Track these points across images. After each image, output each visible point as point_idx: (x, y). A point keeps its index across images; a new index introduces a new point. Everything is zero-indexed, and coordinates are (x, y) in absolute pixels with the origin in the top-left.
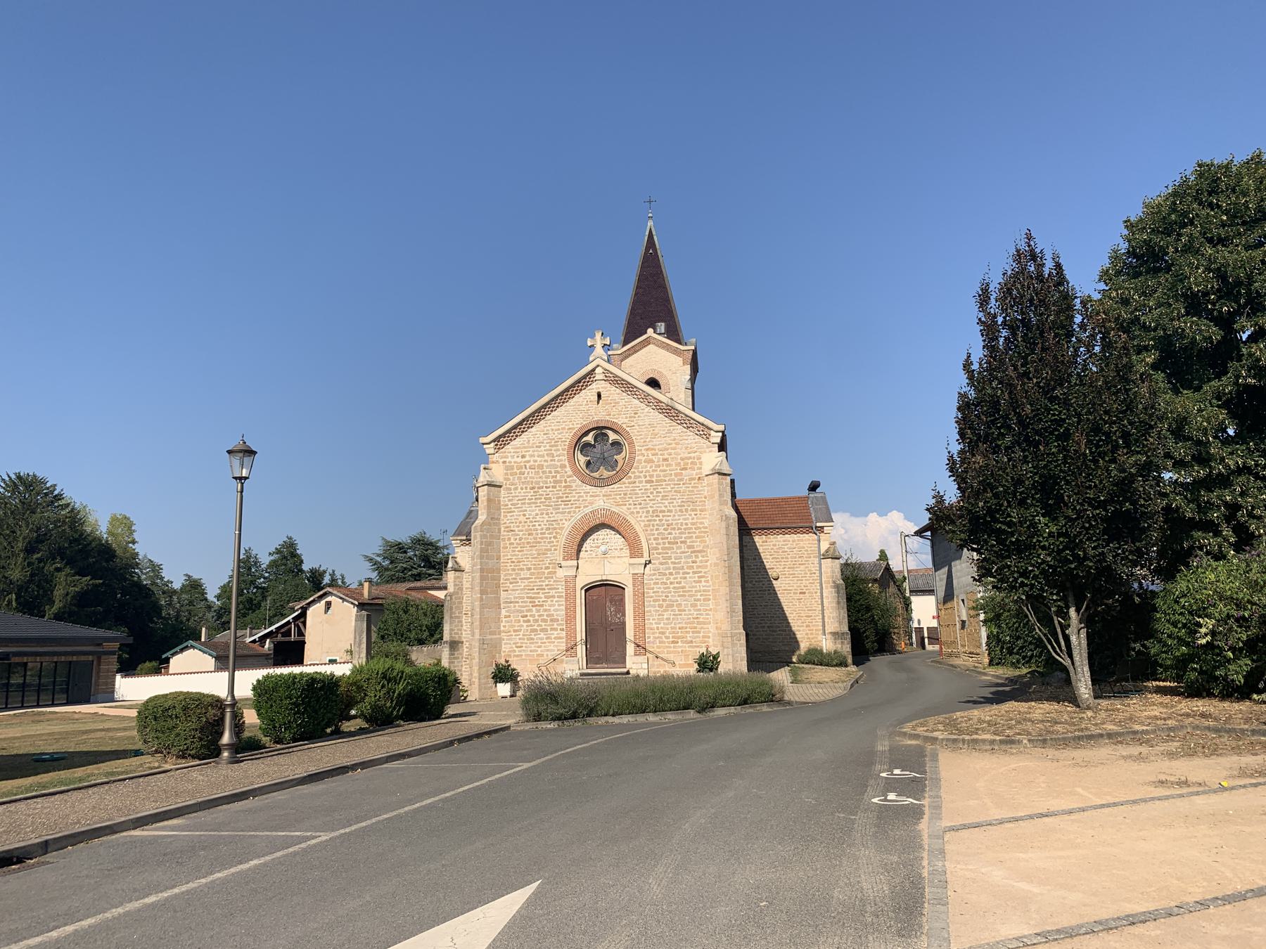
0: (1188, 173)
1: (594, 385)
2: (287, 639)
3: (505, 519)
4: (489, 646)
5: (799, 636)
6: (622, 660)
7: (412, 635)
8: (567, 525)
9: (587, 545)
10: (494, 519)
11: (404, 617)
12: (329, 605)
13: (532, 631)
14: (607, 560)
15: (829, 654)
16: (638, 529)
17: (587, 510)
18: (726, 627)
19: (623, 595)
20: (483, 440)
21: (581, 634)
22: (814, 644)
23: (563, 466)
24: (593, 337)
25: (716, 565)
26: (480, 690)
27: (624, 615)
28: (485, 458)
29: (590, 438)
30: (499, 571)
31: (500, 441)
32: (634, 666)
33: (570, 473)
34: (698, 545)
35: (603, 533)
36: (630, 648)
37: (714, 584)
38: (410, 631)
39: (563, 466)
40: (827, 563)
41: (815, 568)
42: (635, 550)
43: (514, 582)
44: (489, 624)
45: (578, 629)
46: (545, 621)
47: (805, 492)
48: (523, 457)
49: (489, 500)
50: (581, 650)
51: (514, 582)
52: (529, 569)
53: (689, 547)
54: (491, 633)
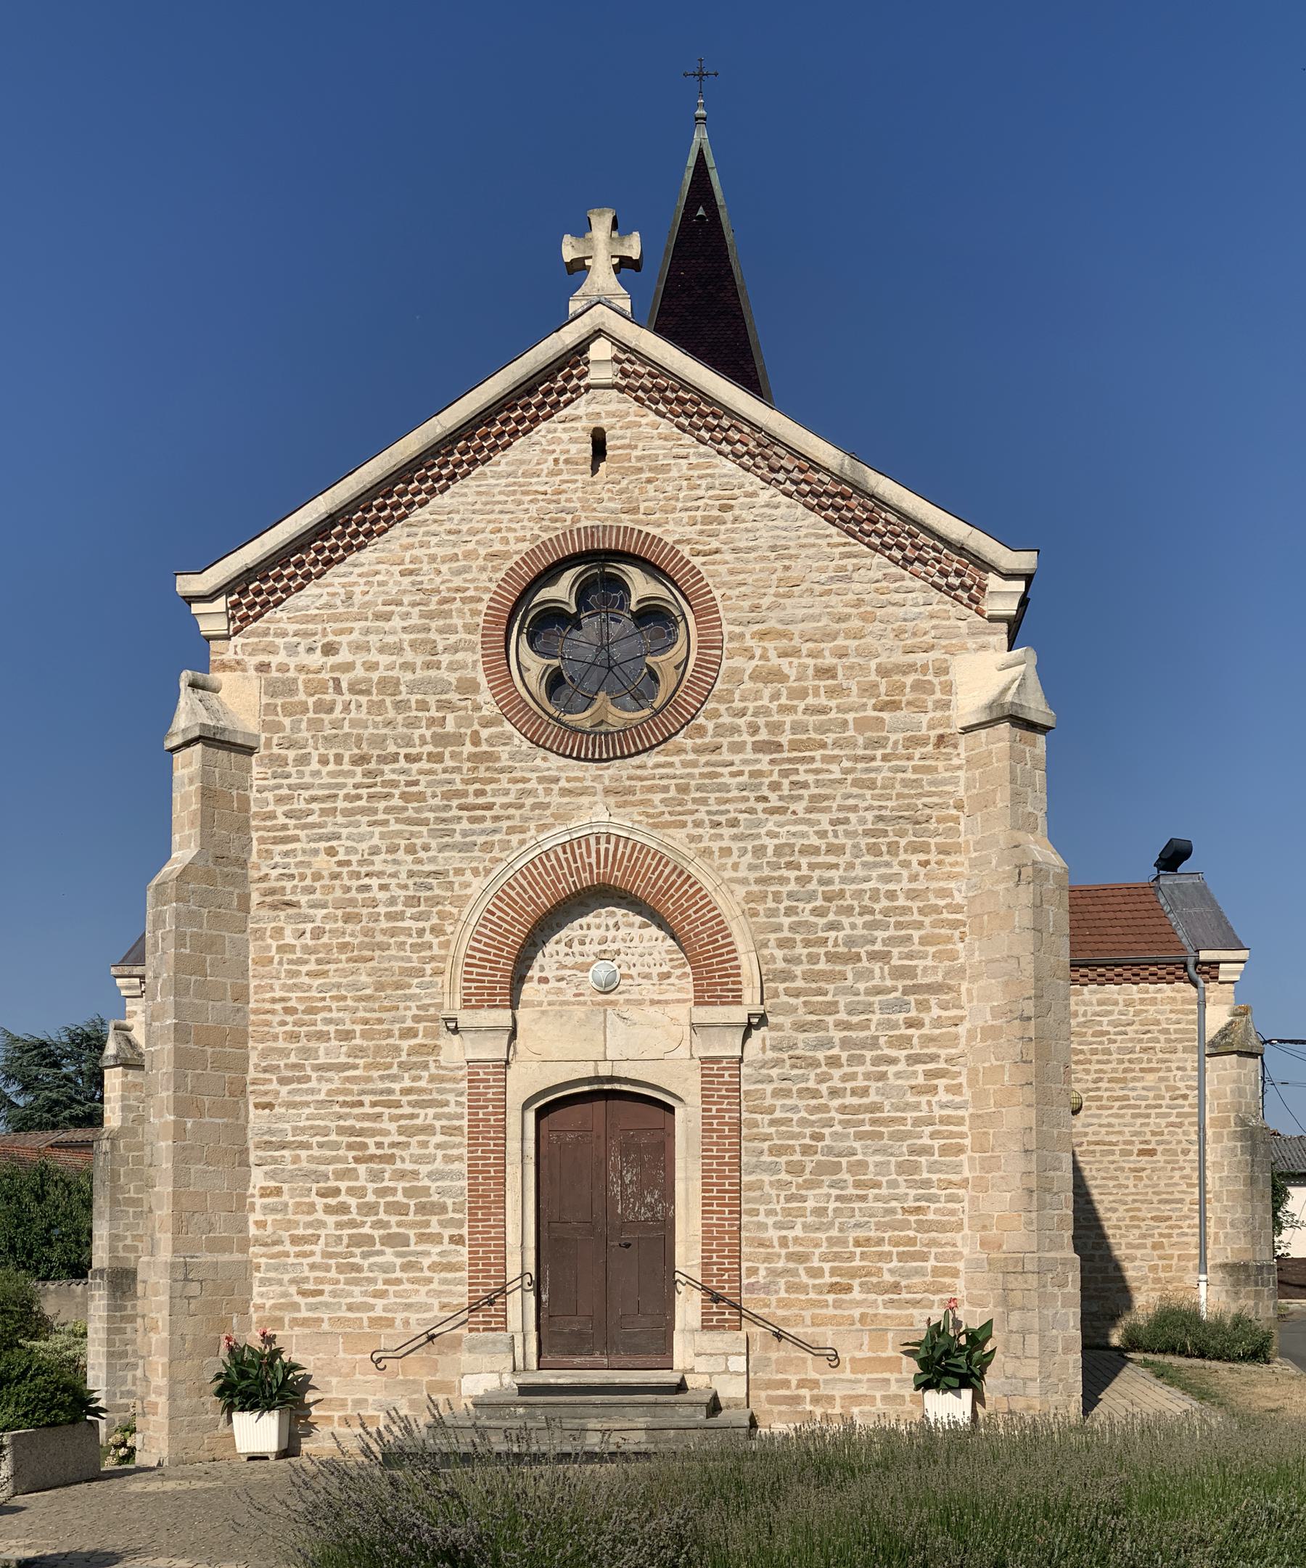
0: (139, 1437)
1: (581, 407)
3: (264, 865)
4: (211, 1286)
5: (1130, 1273)
7: (56, 1254)
10: (224, 861)
11: (35, 1209)
13: (356, 1241)
14: (610, 1010)
15: (1217, 1327)
16: (728, 904)
17: (555, 837)
18: (1017, 1238)
19: (667, 1134)
20: (189, 584)
21: (519, 1257)
22: (1179, 1298)
23: (468, 687)
24: (582, 229)
25: (990, 1033)
27: (668, 1195)
28: (197, 652)
29: (562, 591)
30: (241, 1038)
31: (254, 592)
32: (701, 1365)
33: (490, 710)
34: (929, 969)
35: (599, 925)
36: (688, 1307)
37: (978, 1097)
38: (49, 1243)
39: (468, 687)
40: (1224, 1070)
41: (1184, 1083)
42: (713, 980)
43: (295, 1076)
44: (213, 1209)
45: (513, 1238)
46: (400, 1209)
47: (1145, 871)
49: (207, 794)
50: (520, 1309)
51: (295, 1076)
52: (346, 1036)
53: (899, 973)
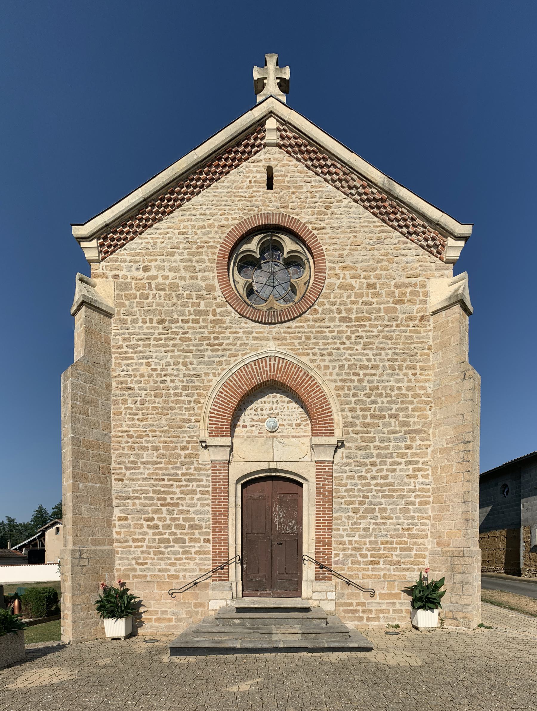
1: (262, 155)
2: (35, 548)
6: (295, 589)
8: (215, 382)
9: (247, 417)
12: (58, 530)
13: (162, 541)
14: (275, 439)
16: (329, 389)
20: (79, 231)
21: (234, 549)
23: (210, 289)
24: (264, 64)
26: (74, 628)
27: (300, 522)
28: (85, 266)
30: (108, 448)
31: (111, 237)
33: (221, 299)
34: (416, 423)
36: (309, 571)
45: (231, 540)
46: (182, 527)
48: (146, 269)
50: (235, 571)
52: (156, 448)
53: (403, 424)
54: (95, 542)
